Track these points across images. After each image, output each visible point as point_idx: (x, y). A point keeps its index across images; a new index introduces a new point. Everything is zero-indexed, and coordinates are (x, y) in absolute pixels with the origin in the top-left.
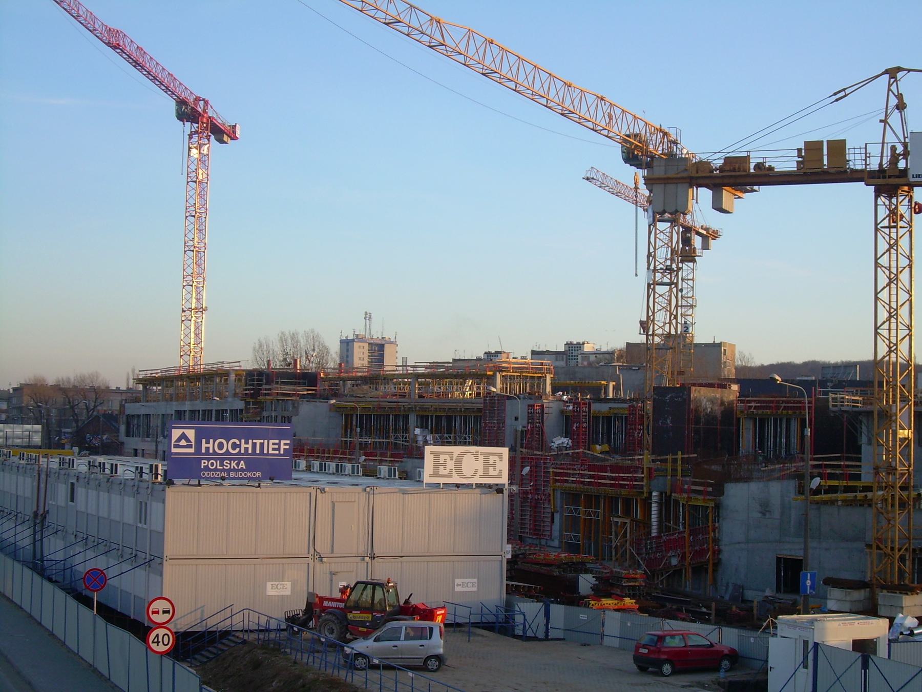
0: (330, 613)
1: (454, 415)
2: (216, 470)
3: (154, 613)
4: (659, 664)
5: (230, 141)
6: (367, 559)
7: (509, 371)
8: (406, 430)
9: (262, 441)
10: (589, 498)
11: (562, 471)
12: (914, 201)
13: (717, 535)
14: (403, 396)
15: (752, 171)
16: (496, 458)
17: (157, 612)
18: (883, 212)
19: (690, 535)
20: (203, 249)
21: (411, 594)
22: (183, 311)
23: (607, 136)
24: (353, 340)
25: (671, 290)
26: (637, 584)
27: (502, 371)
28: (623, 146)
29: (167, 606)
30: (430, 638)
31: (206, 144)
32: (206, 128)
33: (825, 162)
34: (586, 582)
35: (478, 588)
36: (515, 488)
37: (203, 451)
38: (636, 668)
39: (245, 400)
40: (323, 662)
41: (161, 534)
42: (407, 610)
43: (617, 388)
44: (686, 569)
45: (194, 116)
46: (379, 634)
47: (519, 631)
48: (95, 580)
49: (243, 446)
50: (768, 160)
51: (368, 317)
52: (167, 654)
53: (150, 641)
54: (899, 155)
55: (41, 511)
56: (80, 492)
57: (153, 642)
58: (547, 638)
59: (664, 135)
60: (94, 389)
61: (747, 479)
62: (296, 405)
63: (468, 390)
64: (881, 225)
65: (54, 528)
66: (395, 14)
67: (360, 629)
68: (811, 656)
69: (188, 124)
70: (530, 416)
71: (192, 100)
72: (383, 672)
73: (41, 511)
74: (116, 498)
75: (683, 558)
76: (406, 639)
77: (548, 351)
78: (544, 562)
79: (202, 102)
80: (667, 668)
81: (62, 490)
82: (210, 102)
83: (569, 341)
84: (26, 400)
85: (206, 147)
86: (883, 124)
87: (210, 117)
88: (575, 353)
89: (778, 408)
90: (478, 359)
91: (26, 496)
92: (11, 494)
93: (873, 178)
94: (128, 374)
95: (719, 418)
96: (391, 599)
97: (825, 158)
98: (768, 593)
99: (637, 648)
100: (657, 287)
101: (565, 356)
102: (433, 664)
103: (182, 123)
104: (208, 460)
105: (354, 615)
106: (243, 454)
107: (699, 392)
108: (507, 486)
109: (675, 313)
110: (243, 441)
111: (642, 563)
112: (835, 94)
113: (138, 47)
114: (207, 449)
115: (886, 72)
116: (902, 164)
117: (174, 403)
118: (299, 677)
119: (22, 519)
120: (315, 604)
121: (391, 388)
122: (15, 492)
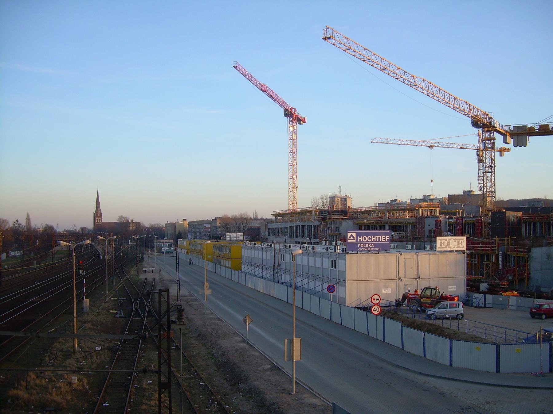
0: (414, 299)
3: (373, 300)
5: (303, 124)
6: (417, 279)
7: (424, 207)
9: (379, 237)
13: (528, 267)
14: (382, 218)
15: (551, 130)
16: (462, 241)
17: (375, 300)
20: (296, 165)
21: (444, 292)
24: (334, 197)
25: (492, 174)
27: (422, 207)
28: (472, 120)
30: (459, 307)
31: (295, 125)
34: (484, 286)
35: (457, 289)
36: (469, 252)
37: (359, 241)
40: (420, 317)
42: (443, 298)
43: (462, 213)
44: (516, 280)
48: (331, 289)
49: (373, 238)
51: (340, 188)
52: (379, 315)
53: (373, 310)
55: (277, 265)
57: (373, 311)
58: (485, 307)
59: (487, 116)
61: (541, 246)
62: (341, 223)
63: (406, 215)
67: (426, 305)
70: (436, 225)
73: (277, 265)
75: (514, 276)
76: (449, 308)
77: (416, 199)
79: (294, 109)
80: (544, 316)
82: (296, 109)
83: (424, 195)
85: (295, 126)
87: (296, 115)
88: (427, 199)
89: (536, 218)
90: (388, 203)
92: (252, 257)
99: (531, 309)
100: (487, 173)
101: (423, 201)
102: (460, 317)
103: (287, 118)
104: (361, 244)
107: (509, 213)
108: (466, 251)
109: (494, 183)
110: (373, 237)
111: (496, 279)
113: (271, 90)
114: (360, 240)
117: (289, 223)
120: (408, 296)
122: (262, 258)
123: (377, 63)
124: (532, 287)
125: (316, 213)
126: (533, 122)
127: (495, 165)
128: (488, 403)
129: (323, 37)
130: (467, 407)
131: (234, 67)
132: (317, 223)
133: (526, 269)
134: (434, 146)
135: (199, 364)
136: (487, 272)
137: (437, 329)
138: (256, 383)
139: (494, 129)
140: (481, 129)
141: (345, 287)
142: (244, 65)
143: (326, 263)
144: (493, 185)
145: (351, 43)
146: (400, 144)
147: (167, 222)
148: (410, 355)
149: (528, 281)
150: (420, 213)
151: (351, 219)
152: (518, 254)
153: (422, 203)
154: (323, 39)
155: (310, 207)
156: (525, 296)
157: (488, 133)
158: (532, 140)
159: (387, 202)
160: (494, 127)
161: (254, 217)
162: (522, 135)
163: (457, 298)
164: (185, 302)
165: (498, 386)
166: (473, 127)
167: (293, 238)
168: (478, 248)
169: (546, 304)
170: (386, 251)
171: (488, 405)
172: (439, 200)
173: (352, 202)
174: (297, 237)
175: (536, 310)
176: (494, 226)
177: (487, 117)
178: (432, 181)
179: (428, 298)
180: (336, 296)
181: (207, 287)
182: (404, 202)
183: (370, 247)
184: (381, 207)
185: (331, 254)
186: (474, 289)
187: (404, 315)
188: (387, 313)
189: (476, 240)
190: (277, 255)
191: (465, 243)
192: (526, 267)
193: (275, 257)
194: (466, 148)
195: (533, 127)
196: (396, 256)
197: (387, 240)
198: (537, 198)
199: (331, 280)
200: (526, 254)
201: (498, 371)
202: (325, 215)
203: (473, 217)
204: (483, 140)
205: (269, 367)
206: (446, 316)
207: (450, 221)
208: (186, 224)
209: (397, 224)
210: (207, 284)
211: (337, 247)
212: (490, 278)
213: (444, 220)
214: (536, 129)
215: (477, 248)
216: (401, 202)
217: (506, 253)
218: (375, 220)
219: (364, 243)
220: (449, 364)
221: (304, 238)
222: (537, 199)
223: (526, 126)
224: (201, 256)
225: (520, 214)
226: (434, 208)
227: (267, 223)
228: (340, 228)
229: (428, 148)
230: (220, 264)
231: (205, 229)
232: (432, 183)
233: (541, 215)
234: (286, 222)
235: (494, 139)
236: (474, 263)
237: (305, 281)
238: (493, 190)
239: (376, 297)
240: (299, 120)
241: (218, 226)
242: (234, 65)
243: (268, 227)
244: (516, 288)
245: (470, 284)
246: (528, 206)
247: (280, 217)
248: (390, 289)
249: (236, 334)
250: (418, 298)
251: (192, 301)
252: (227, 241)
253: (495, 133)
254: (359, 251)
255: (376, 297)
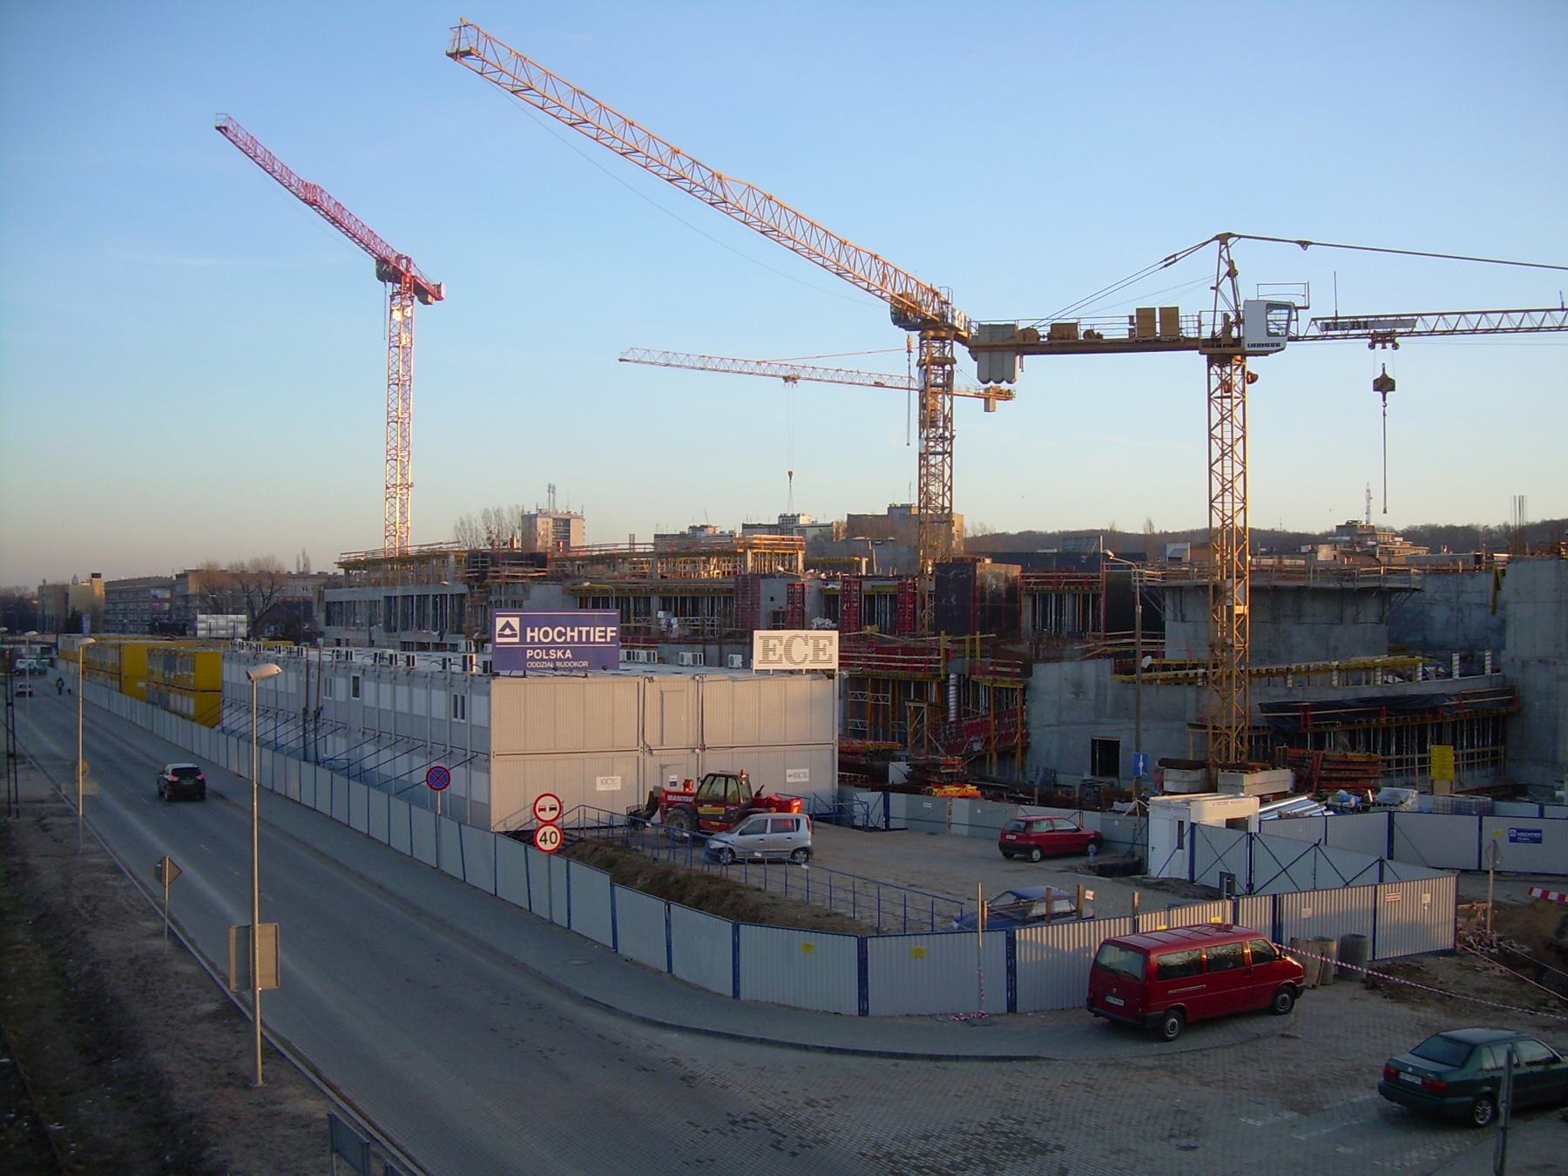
0: (679, 808)
1: (700, 596)
2: (542, 660)
3: (540, 810)
4: (1028, 850)
5: (435, 302)
6: (697, 750)
7: (760, 548)
8: (648, 613)
9: (588, 629)
10: (876, 682)
11: (846, 654)
12: (1247, 369)
13: (1025, 718)
14: (644, 576)
15: (1082, 338)
17: (544, 810)
18: (1215, 382)
19: (995, 719)
20: (407, 420)
21: (763, 787)
22: (387, 488)
23: (880, 297)
24: (536, 516)
25: (944, 460)
26: (955, 770)
29: (555, 803)
31: (408, 306)
32: (409, 289)
33: (1158, 330)
34: (897, 771)
37: (529, 640)
38: (1001, 855)
39: (468, 584)
40: (689, 859)
41: (486, 730)
42: (760, 803)
43: (870, 565)
45: (396, 276)
46: (743, 828)
47: (858, 823)
49: (569, 634)
50: (1096, 327)
51: (551, 489)
52: (558, 851)
53: (538, 838)
54: (1232, 323)
55: (313, 708)
56: (368, 687)
57: (541, 840)
58: (888, 829)
59: (934, 295)
60: (271, 574)
61: (1058, 659)
62: (527, 588)
63: (713, 570)
64: (1215, 395)
65: (331, 725)
66: (678, 168)
67: (712, 823)
68: (1186, 840)
69: (390, 284)
70: (791, 598)
71: (393, 258)
72: (768, 866)
73: (313, 708)
74: (420, 693)
75: (988, 741)
76: (772, 832)
77: (759, 524)
78: (849, 750)
79: (404, 261)
80: (1036, 854)
81: (342, 687)
82: (413, 259)
83: (783, 513)
84: (193, 588)
85: (409, 309)
86: (1214, 291)
87: (413, 277)
88: (790, 526)
90: (682, 535)
91: (290, 691)
92: (267, 690)
93: (1206, 346)
94: (298, 557)
95: (1004, 596)
96: (744, 792)
97: (1158, 325)
98: (1087, 776)
99: (1004, 835)
103: (383, 283)
104: (534, 649)
105: (705, 810)
106: (568, 643)
108: (837, 671)
109: (949, 484)
110: (569, 629)
111: (940, 748)
112: (1166, 260)
114: (533, 638)
115: (1217, 238)
116: (1235, 334)
117: (384, 588)
118: (668, 874)
119: (285, 717)
120: (662, 798)
121: (626, 568)
122: (273, 688)
123: (611, 132)
124: (1034, 773)
125: (459, 562)
126: (1035, 315)
127: (954, 433)
128: (810, 1103)
129: (449, 51)
130: (750, 1117)
131: (218, 128)
132: (463, 589)
133: (1019, 722)
134: (799, 378)
135: (15, 1003)
136: (916, 731)
137: (727, 893)
138: (158, 1056)
139: (953, 333)
140: (918, 332)
141: (488, 771)
142: (251, 124)
143: (440, 703)
144: (946, 488)
145: (534, 72)
146: (702, 369)
147: (44, 581)
148: (633, 965)
149: (1022, 755)
150: (750, 564)
151: (557, 578)
152: (996, 680)
153: (755, 536)
154: (451, 55)
155: (441, 543)
156: (1007, 797)
157: (938, 345)
158: (1032, 368)
159: (678, 533)
160: (952, 327)
161: (299, 569)
162: (1003, 351)
163: (798, 803)
164: (32, 820)
165: (854, 1052)
166: (897, 327)
167: (395, 631)
168: (894, 664)
169: (1043, 820)
170: (605, 669)
171: (811, 1110)
172: (818, 529)
173: (585, 530)
174: (405, 629)
175: (1014, 837)
176: (944, 603)
177: (936, 300)
178: (790, 474)
179: (717, 801)
180: (466, 799)
181: (83, 773)
182: (727, 532)
183: (560, 660)
184: (643, 546)
185: (451, 679)
186: (862, 777)
187: (648, 853)
188: (602, 847)
189: (890, 641)
190: (313, 681)
191: (833, 650)
192: (1019, 718)
193: (307, 685)
194: (890, 385)
195: (1035, 330)
196: (636, 684)
197: (611, 637)
198: (1099, 528)
199: (451, 752)
200: (1020, 682)
201: (863, 1012)
202: (485, 567)
203: (894, 577)
204: (922, 362)
205: (212, 1007)
206: (756, 854)
207: (830, 586)
208: (99, 590)
209: (683, 595)
210: (86, 764)
211: (471, 658)
212: (923, 746)
213: (812, 584)
214: (1041, 334)
215: (890, 664)
216: (718, 532)
217: (968, 679)
218: (624, 583)
219: (544, 648)
220: (730, 993)
221: (425, 631)
222: (1267, 531)
223: (1014, 325)
224: (118, 683)
225: (1015, 571)
226: (788, 552)
227: (322, 589)
228: (524, 602)
229: (783, 381)
230: (166, 708)
231: (155, 604)
232: (791, 478)
233: (1076, 574)
234: (378, 584)
235: (953, 361)
236: (883, 705)
237: (386, 754)
238: (947, 504)
239: (548, 802)
240: (423, 293)
241: (194, 596)
242: (218, 125)
243: (327, 600)
244: (991, 773)
245: (862, 763)
246: (1061, 550)
247: (358, 572)
248: (619, 778)
249: (150, 913)
250: (691, 803)
251: (53, 815)
252: (199, 639)
253: (955, 343)
254: (528, 669)
255: (548, 802)
